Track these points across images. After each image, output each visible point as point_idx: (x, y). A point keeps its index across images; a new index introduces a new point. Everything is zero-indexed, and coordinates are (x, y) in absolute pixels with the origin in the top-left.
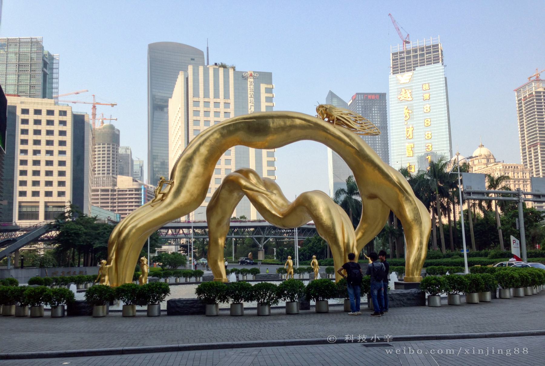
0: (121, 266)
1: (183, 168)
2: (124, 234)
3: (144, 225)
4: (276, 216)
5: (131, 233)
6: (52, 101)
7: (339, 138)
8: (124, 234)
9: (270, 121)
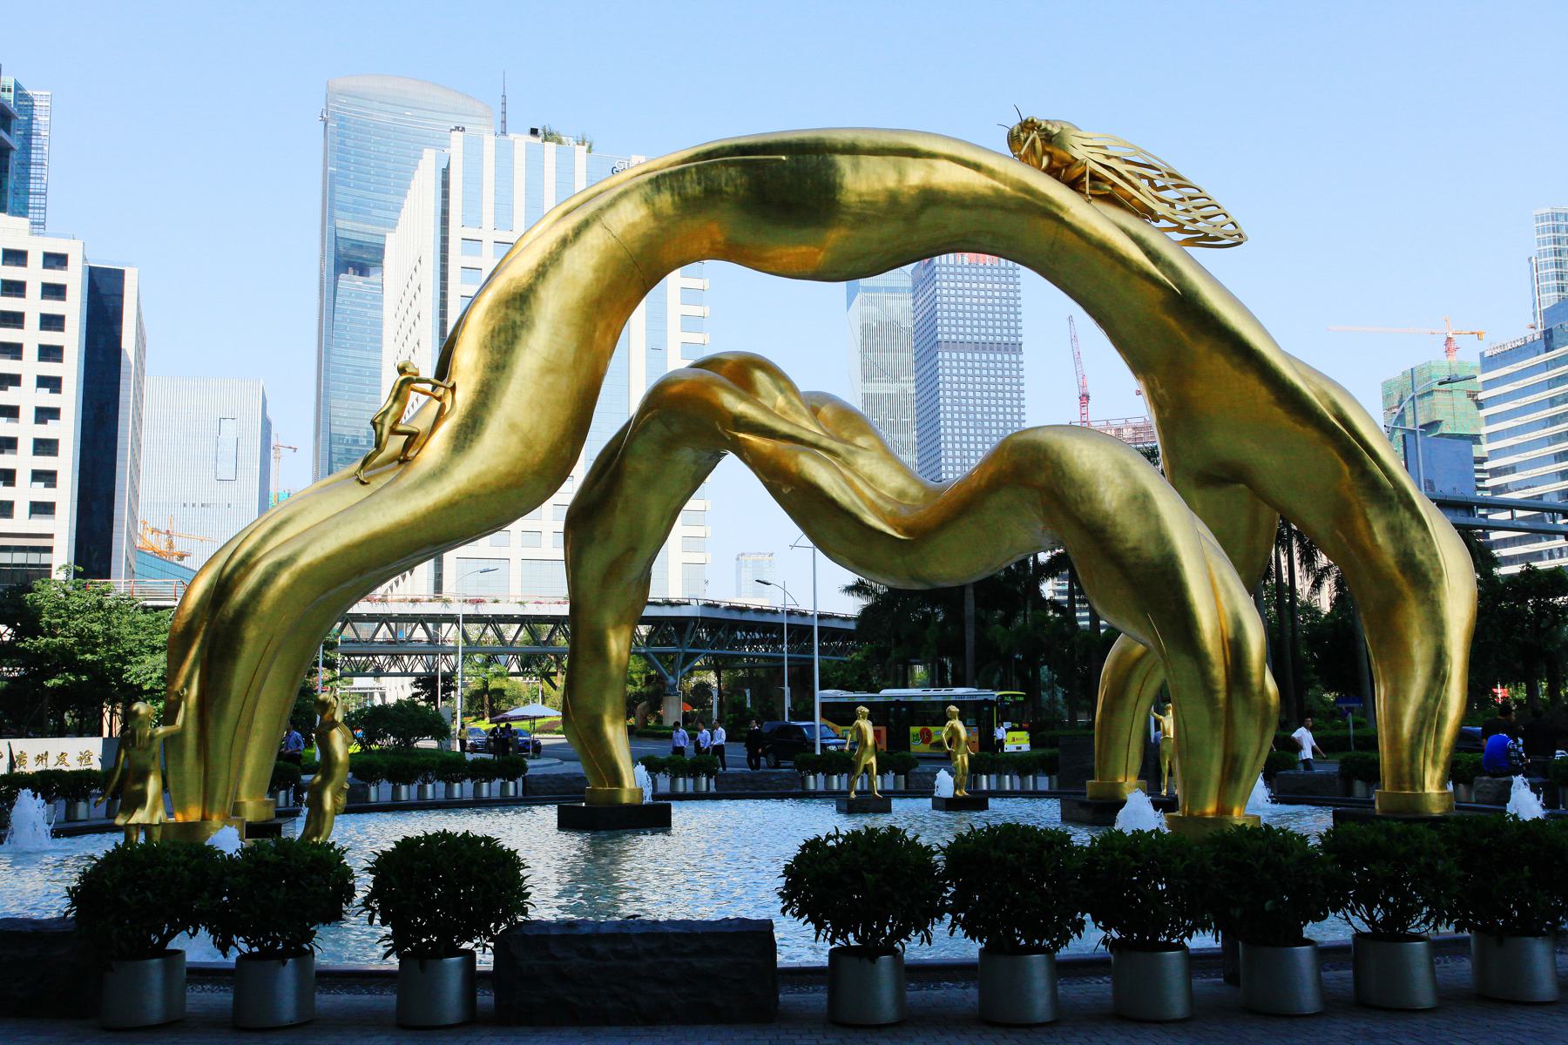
0: (224, 733)
1: (494, 334)
2: (240, 594)
3: (329, 559)
4: (882, 533)
5: (273, 592)
6: (23, 223)
7: (1104, 248)
8: (240, 594)
9: (843, 161)
